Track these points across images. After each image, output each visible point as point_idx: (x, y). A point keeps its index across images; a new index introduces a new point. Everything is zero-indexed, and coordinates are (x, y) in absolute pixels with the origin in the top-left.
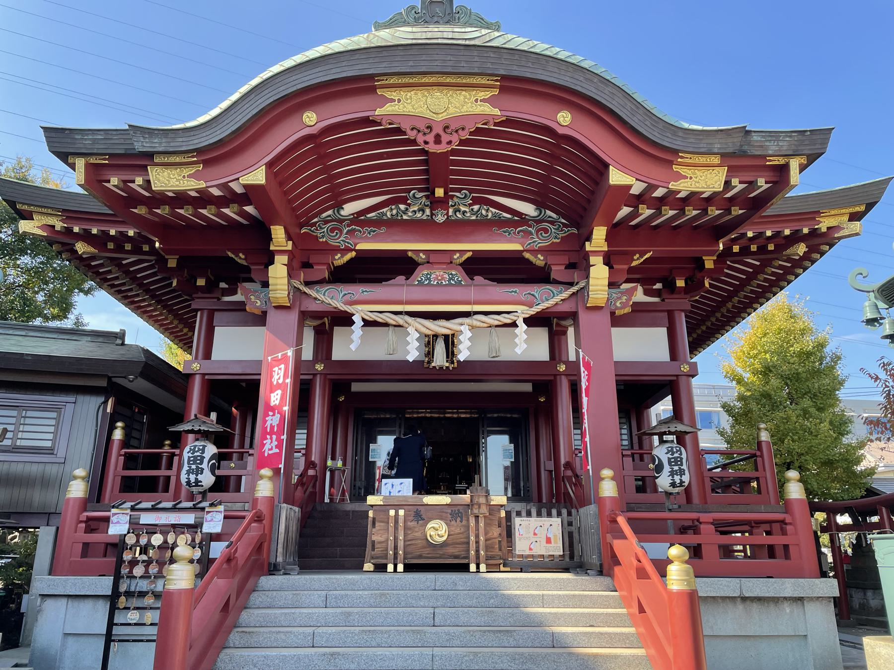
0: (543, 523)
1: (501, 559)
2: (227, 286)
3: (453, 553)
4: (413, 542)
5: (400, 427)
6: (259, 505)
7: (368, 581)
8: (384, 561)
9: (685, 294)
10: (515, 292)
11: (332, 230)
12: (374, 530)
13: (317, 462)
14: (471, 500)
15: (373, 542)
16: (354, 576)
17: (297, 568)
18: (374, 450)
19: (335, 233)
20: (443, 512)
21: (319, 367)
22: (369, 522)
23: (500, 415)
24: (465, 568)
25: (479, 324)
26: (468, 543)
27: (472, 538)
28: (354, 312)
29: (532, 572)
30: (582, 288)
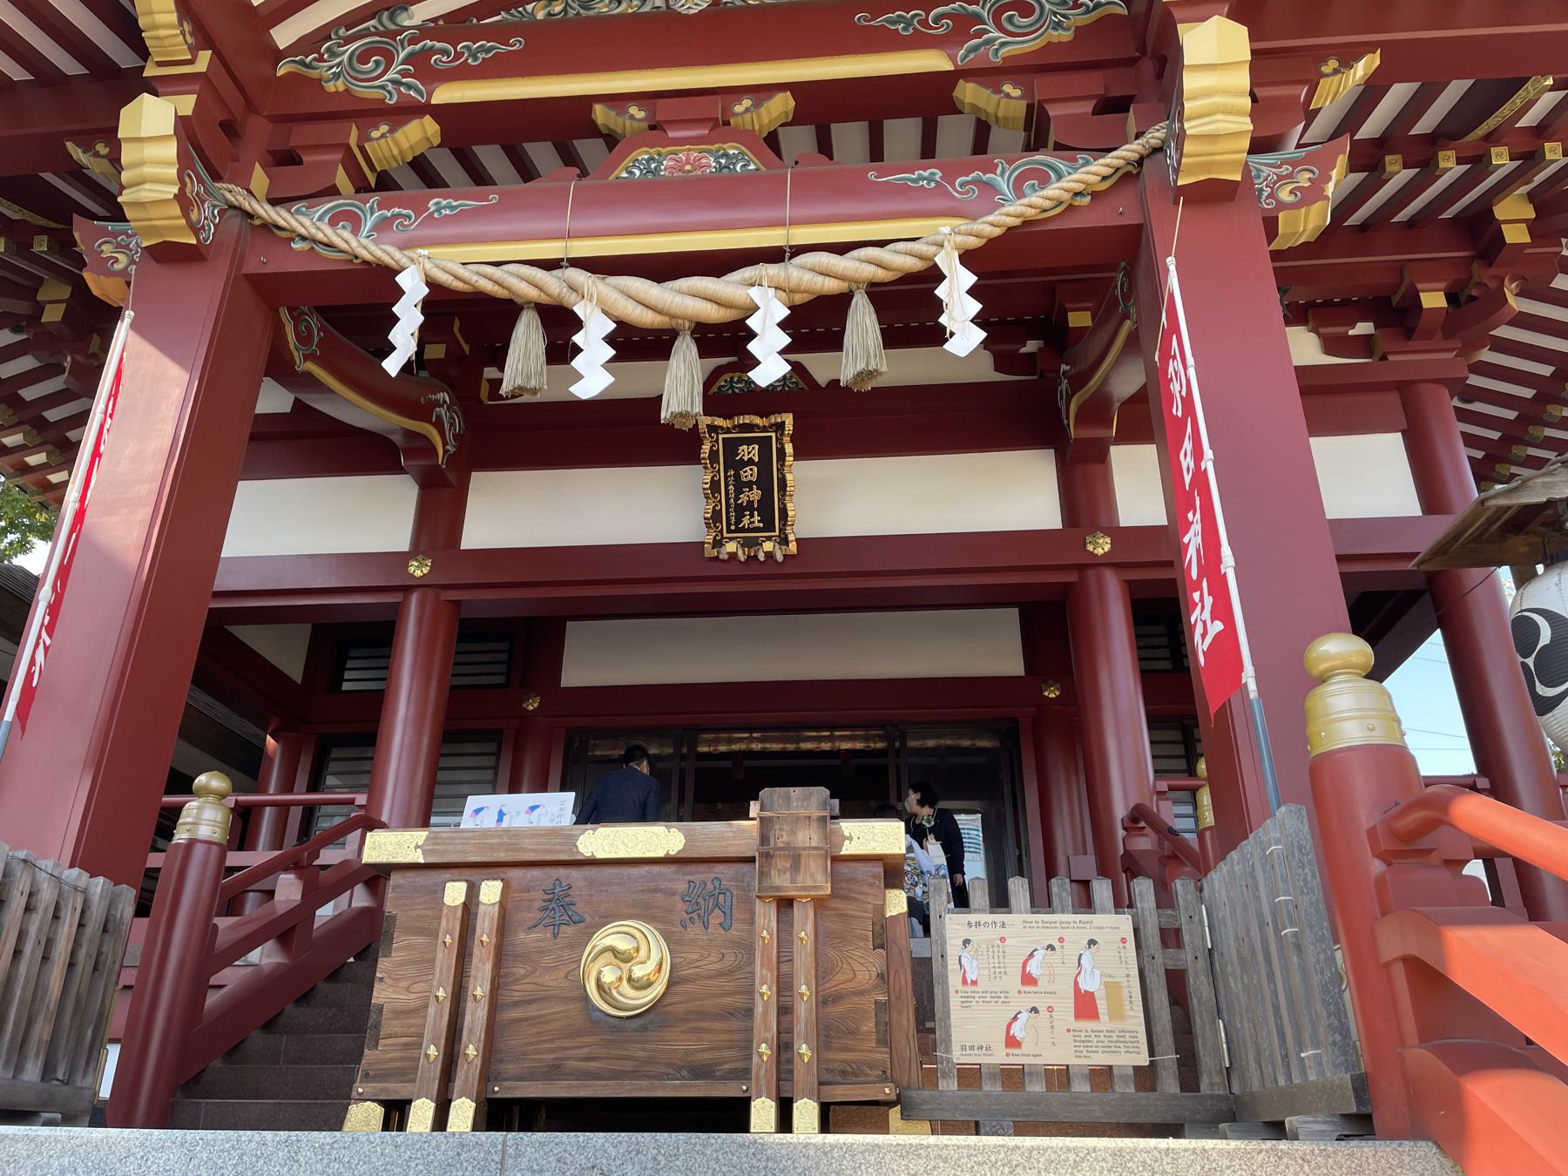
0: (1061, 933)
1: (884, 1079)
4: (533, 1010)
9: (1445, 338)
10: (929, 180)
11: (364, 57)
14: (764, 839)
19: (371, 65)
20: (657, 890)
23: (942, 742)
24: (732, 1116)
26: (749, 1013)
27: (766, 990)
28: (404, 261)
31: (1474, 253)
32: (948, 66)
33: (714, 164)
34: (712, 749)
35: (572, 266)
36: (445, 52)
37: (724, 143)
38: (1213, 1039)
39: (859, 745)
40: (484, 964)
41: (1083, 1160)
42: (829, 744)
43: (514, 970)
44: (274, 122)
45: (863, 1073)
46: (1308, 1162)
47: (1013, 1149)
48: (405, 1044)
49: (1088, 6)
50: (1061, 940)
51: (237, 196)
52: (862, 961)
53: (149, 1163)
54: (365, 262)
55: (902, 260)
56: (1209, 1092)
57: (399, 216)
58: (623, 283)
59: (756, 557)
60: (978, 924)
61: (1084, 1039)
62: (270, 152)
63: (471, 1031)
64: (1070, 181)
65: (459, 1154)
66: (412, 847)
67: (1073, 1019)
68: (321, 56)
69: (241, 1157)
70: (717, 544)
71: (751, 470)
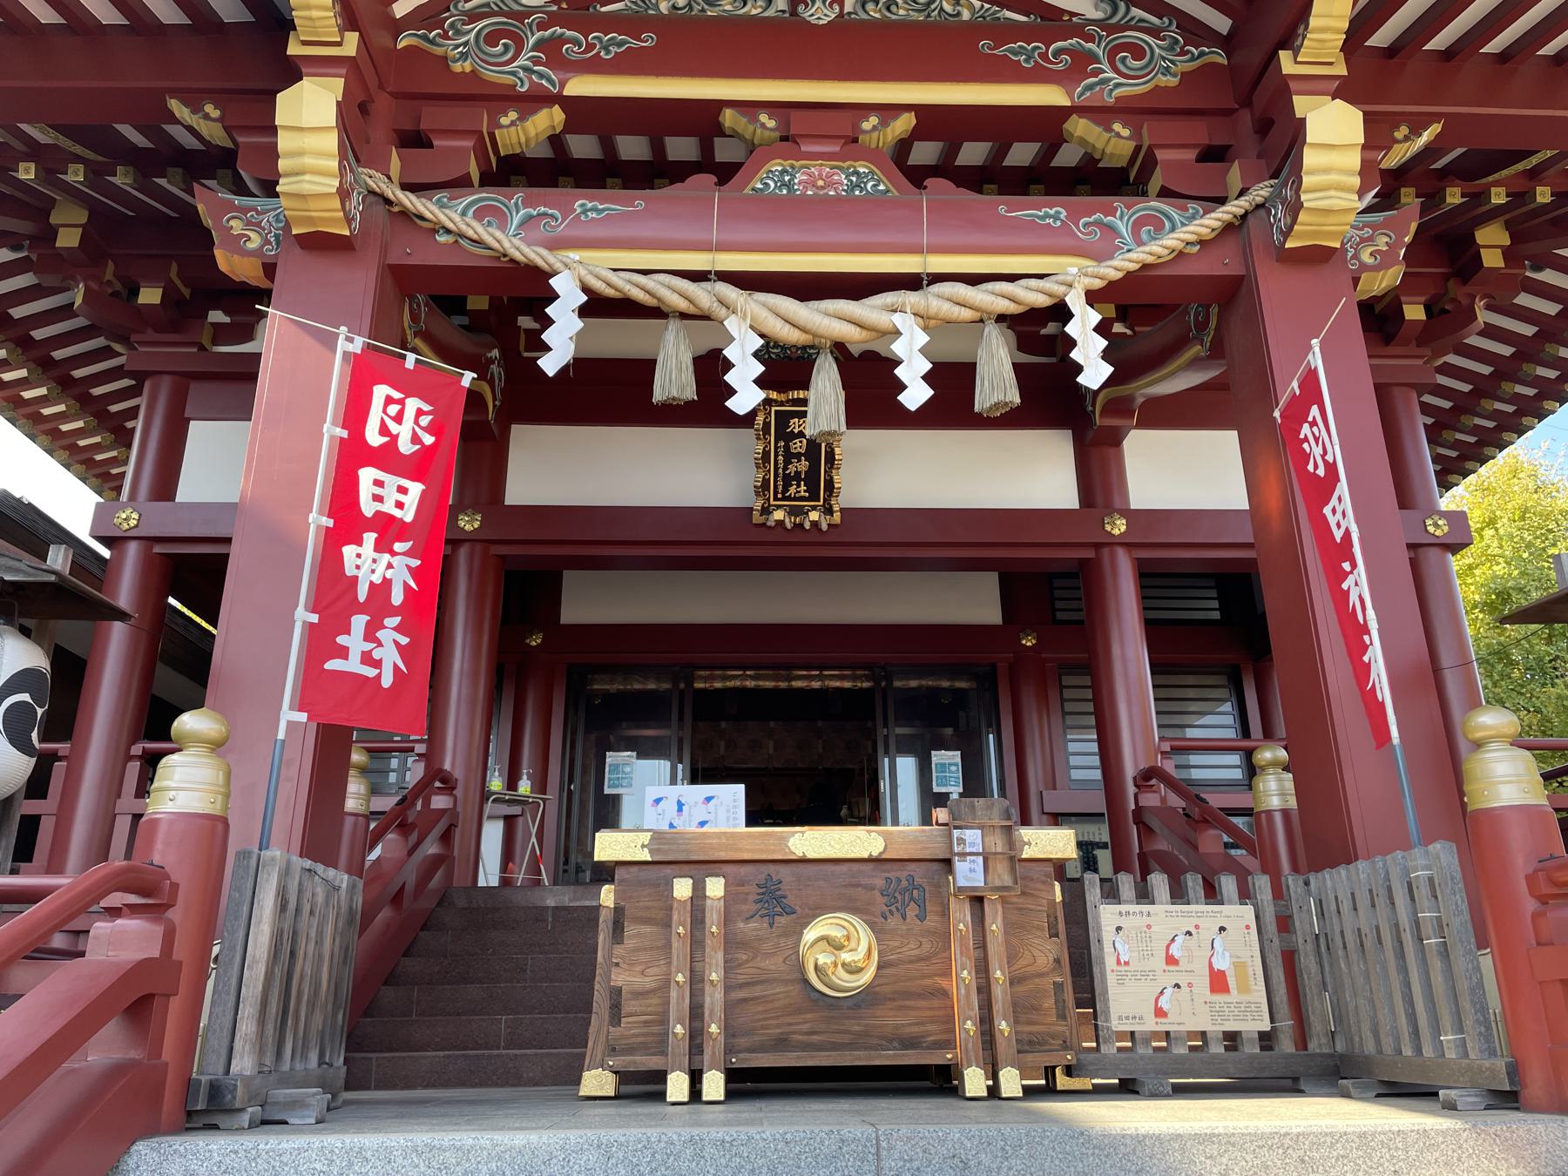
0: (1196, 921)
2: (227, 320)
3: (897, 1027)
4: (757, 991)
5: (681, 728)
6: (159, 845)
7: (592, 1157)
8: (652, 1062)
9: (1418, 346)
10: (1056, 217)
11: (492, 38)
12: (619, 950)
13: (458, 774)
15: (617, 992)
16: (533, 1137)
17: (317, 1098)
18: (616, 767)
19: (499, 48)
20: (858, 885)
21: (468, 523)
22: (602, 926)
23: (924, 683)
25: (948, 310)
28: (558, 266)
29: (1180, 1091)
30: (1259, 206)
31: (1451, 270)
32: (1064, 101)
33: (845, 182)
34: (707, 685)
35: (720, 280)
36: (577, 43)
37: (855, 161)
38: (1320, 1008)
39: (847, 685)
40: (716, 952)
41: (1337, 1141)
42: (819, 683)
43: (736, 955)
44: (396, 98)
45: (1046, 1043)
46: (1498, 1136)
47: (1284, 1135)
48: (645, 1022)
49: (1193, 54)
50: (1197, 927)
51: (378, 182)
52: (1040, 948)
53: (571, 1164)
54: (512, 260)
55: (1033, 296)
56: (1318, 1051)
57: (545, 214)
58: (773, 301)
59: (801, 525)
60: (1128, 913)
61: (1218, 1009)
62: (395, 130)
63: (712, 1012)
64: (1185, 232)
65: (840, 1148)
66: (639, 846)
67: (1209, 993)
68: (446, 32)
69: (653, 1155)
70: (766, 511)
71: (801, 442)
